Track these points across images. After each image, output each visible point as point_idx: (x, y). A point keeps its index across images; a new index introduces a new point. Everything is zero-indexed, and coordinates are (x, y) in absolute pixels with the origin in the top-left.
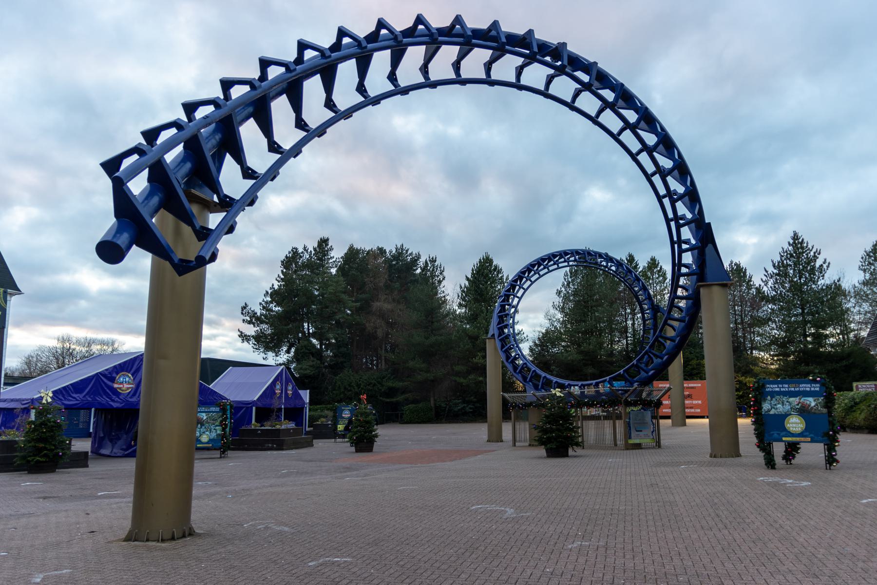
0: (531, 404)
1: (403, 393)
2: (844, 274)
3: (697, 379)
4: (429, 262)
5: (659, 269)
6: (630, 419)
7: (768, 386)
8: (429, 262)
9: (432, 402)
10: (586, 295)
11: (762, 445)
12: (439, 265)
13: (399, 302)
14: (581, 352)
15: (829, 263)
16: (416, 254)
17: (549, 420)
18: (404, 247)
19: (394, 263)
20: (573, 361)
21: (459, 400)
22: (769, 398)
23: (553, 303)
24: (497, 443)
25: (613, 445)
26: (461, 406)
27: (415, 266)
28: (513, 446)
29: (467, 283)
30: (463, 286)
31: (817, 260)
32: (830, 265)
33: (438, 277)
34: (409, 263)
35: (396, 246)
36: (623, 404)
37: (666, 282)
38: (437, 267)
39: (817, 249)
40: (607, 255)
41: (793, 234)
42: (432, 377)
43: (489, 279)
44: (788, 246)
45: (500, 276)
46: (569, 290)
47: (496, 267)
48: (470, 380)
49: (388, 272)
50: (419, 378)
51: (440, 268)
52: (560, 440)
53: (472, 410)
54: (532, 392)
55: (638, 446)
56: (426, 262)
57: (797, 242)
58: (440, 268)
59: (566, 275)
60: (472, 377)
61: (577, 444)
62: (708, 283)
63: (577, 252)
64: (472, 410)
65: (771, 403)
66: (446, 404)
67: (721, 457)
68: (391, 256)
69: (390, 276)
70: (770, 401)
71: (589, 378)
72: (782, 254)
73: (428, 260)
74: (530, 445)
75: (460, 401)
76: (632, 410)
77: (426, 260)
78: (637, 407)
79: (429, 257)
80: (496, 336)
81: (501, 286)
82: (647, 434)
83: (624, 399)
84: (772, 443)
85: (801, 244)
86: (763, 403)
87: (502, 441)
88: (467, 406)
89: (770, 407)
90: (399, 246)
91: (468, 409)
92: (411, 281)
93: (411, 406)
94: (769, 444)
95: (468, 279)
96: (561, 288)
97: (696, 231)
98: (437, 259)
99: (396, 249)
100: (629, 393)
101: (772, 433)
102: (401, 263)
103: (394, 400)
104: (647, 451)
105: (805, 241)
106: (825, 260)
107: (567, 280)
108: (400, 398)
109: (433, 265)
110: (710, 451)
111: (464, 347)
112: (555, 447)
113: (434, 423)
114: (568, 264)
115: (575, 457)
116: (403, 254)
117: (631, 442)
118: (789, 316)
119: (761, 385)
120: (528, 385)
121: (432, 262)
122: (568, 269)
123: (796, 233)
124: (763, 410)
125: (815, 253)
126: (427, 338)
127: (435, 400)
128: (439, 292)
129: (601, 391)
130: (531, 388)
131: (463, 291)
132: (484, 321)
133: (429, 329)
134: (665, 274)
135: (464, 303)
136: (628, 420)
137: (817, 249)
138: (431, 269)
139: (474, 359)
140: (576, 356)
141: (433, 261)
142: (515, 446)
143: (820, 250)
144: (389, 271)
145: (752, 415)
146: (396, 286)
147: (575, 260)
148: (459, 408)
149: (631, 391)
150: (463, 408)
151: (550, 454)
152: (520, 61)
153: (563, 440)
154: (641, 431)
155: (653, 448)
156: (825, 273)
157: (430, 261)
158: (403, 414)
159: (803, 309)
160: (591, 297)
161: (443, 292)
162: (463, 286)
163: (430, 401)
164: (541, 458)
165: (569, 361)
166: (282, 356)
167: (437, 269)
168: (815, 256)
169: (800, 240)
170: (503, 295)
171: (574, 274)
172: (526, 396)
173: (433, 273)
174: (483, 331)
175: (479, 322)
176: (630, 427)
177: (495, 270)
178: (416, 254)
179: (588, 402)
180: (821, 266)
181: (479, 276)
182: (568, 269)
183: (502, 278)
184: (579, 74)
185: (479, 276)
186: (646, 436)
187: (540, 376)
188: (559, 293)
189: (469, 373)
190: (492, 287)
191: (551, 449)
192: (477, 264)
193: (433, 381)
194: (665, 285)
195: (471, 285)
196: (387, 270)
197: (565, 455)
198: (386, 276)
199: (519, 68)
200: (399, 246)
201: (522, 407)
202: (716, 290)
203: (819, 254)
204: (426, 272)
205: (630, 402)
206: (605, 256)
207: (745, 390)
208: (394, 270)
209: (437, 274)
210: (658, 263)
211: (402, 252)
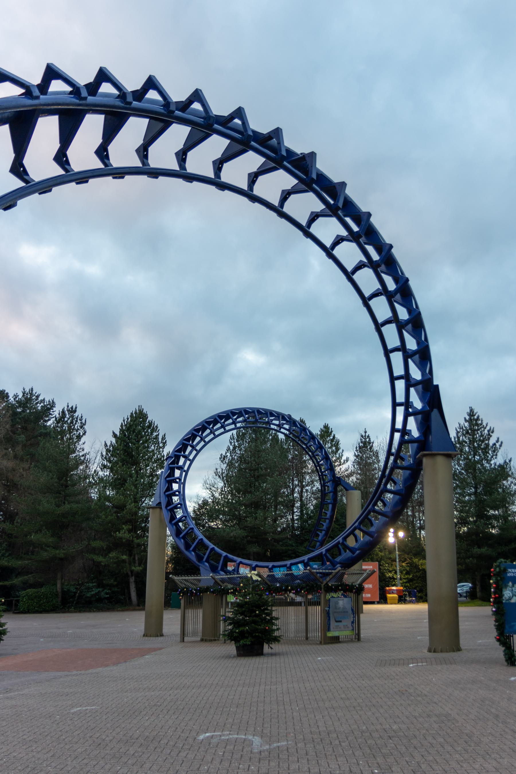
0: (207, 590)
1: (19, 574)
2: (507, 455)
3: (369, 561)
4: (67, 412)
5: (332, 437)
6: (329, 607)
7: (510, 570)
8: (67, 412)
9: (59, 586)
10: (254, 462)
11: (502, 639)
12: (80, 416)
13: (22, 460)
14: (244, 528)
15: (502, 443)
16: (49, 401)
17: (243, 609)
18: (34, 392)
19: (19, 410)
20: (235, 537)
21: (93, 583)
22: (510, 584)
23: (216, 469)
24: (157, 638)
25: (305, 639)
26: (95, 591)
27: (47, 416)
28: (181, 642)
29: (114, 440)
30: (109, 444)
31: (491, 438)
32: (503, 445)
33: (77, 431)
34: (40, 412)
35: (24, 389)
36: (323, 590)
37: (339, 452)
38: (77, 419)
39: (490, 427)
40: (290, 416)
41: (469, 410)
42: (63, 555)
43: (142, 437)
44: (464, 422)
45: (155, 434)
46: (235, 456)
47: (150, 424)
48: (110, 559)
49: (10, 422)
50: (45, 555)
51: (81, 420)
52: (257, 634)
53: (108, 596)
54: (211, 575)
55: (336, 640)
56: (63, 412)
57: (472, 418)
58: (81, 420)
59: (232, 438)
60: (112, 554)
61: (276, 640)
62: (433, 452)
63: (240, 412)
64: (108, 596)
65: (512, 590)
66: (76, 588)
67: (441, 652)
68: (17, 401)
69: (13, 426)
70: (512, 588)
71: (252, 557)
72: (459, 430)
73: (65, 409)
74: (202, 640)
75: (95, 584)
76: (332, 597)
77: (63, 410)
78: (337, 593)
79: (68, 406)
80: (163, 506)
81: (155, 446)
82: (347, 625)
83: (324, 584)
84: (513, 636)
85: (476, 422)
86: (504, 590)
87: (162, 635)
88: (103, 591)
89: (511, 595)
90: (27, 390)
91: (103, 595)
92: (41, 435)
93: (30, 591)
94: (509, 637)
95: (115, 435)
96: (226, 453)
97: (423, 393)
98: (77, 409)
99: (24, 393)
100: (331, 576)
101: (513, 624)
102: (28, 411)
103: (7, 583)
104: (345, 645)
105: (480, 418)
106: (498, 439)
107: (233, 444)
108: (16, 581)
109: (72, 416)
110: (428, 644)
111: (106, 517)
112: (249, 643)
113: (59, 613)
114: (236, 426)
115: (272, 655)
116: (32, 400)
117: (330, 634)
118: (462, 495)
119: (502, 569)
120: (204, 566)
121: (71, 412)
122: (235, 432)
123: (472, 409)
124: (504, 598)
125: (489, 431)
126: (58, 506)
127: (62, 584)
128: (78, 449)
129: (295, 574)
130: (206, 570)
131: (108, 451)
132: (133, 487)
133: (60, 494)
134: (338, 444)
135: (108, 464)
136: (327, 609)
137: (490, 427)
138: (69, 421)
139: (117, 533)
140: (240, 532)
141: (72, 411)
142: (183, 641)
143: (494, 428)
144: (12, 420)
145: (492, 604)
146: (20, 439)
147: (244, 421)
148: (92, 593)
149: (333, 574)
150: (98, 593)
151: (242, 652)
152: (320, 207)
153: (260, 635)
154: (341, 621)
155: (352, 641)
156: (498, 452)
157: (68, 411)
158: (18, 601)
159: (476, 488)
160: (258, 465)
161: (83, 450)
162: (109, 444)
163: (55, 584)
164: (229, 657)
165: (231, 537)
166: (179, 512)
167: (77, 421)
168: (489, 434)
169: (476, 417)
170: (173, 456)
171: (241, 437)
172: (199, 581)
173: (71, 427)
174: (131, 499)
175: (127, 488)
176: (329, 617)
177: (149, 427)
178: (49, 401)
179: (281, 587)
180: (495, 444)
181: (130, 433)
182: (235, 432)
183: (157, 437)
184: (370, 249)
185: (130, 433)
186: (346, 627)
187: (220, 555)
188: (223, 458)
189: (109, 550)
190: (145, 447)
191: (245, 646)
192: (128, 419)
193: (61, 559)
194: (337, 456)
195: (119, 443)
196: (10, 419)
197: (260, 653)
198: (8, 426)
199: (253, 175)
200: (27, 390)
201: (196, 593)
202: (440, 460)
203: (493, 432)
204: (63, 424)
205: (331, 587)
206: (288, 418)
207: (415, 573)
208: (20, 419)
209: (76, 427)
210: (332, 431)
211: (31, 397)
